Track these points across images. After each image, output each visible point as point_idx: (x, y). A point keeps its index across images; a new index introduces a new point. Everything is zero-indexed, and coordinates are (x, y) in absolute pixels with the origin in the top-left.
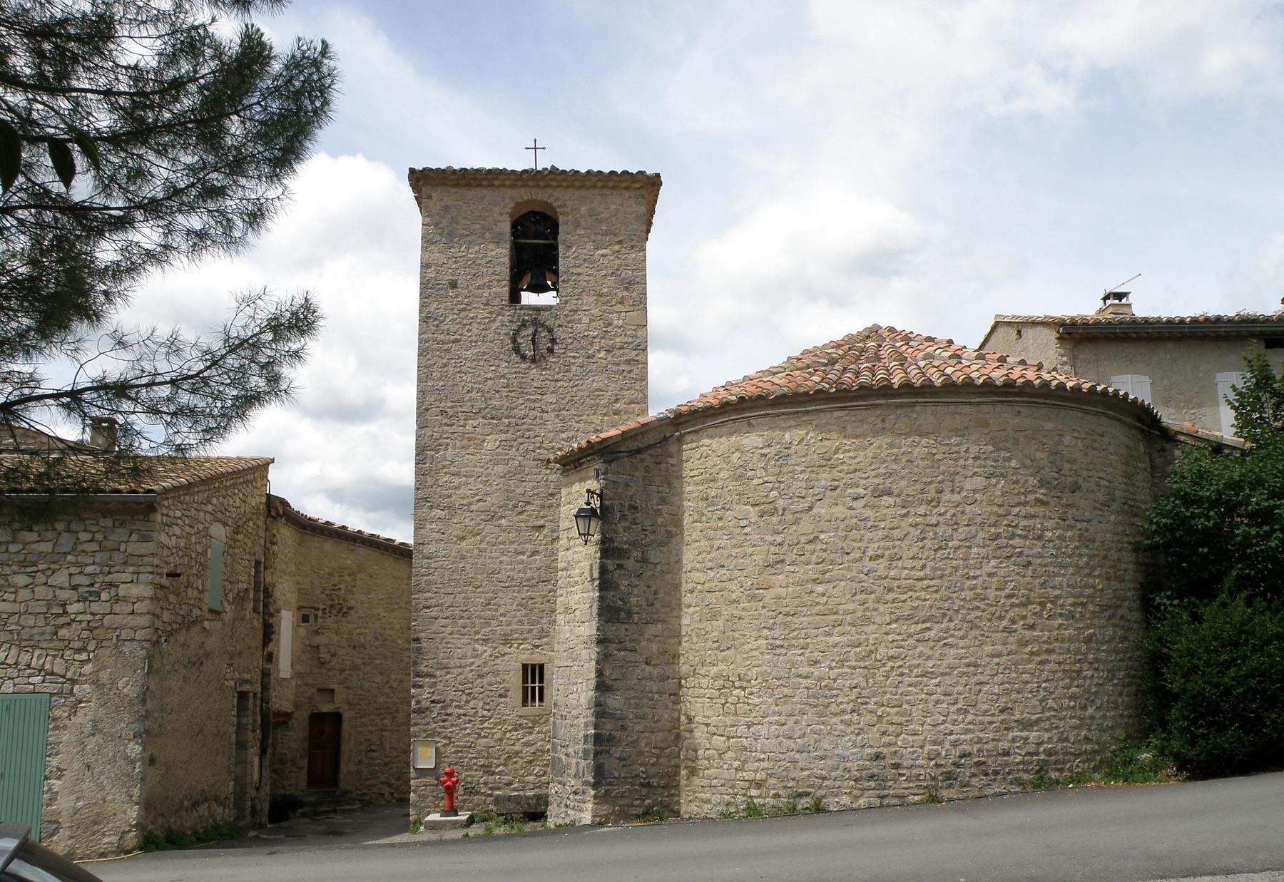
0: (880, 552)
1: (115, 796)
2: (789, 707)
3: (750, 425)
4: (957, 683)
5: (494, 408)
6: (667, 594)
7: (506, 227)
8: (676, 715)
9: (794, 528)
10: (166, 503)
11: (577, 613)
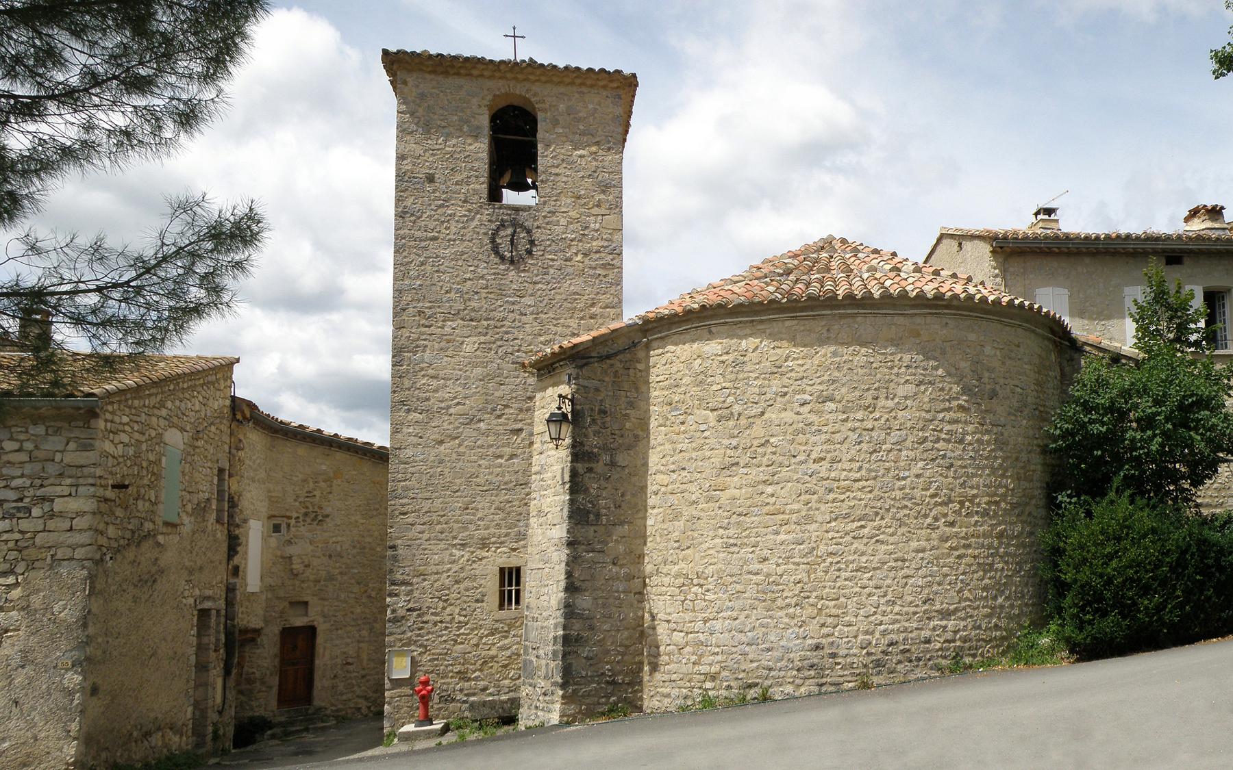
0: (822, 455)
1: (49, 732)
3: (710, 332)
4: (887, 576)
5: (473, 310)
6: (633, 495)
7: (484, 121)
8: (640, 614)
9: (748, 432)
10: (110, 408)
11: (549, 516)
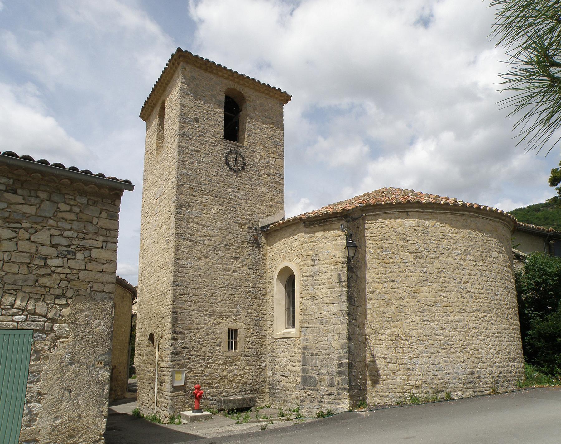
0: (468, 280)
2: (432, 349)
3: (408, 215)
5: (217, 192)
7: (222, 98)
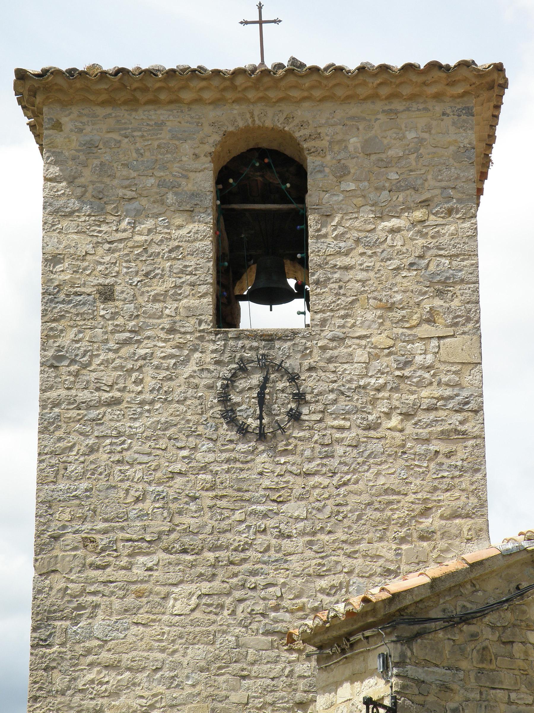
5: (187, 531)
7: (204, 181)
